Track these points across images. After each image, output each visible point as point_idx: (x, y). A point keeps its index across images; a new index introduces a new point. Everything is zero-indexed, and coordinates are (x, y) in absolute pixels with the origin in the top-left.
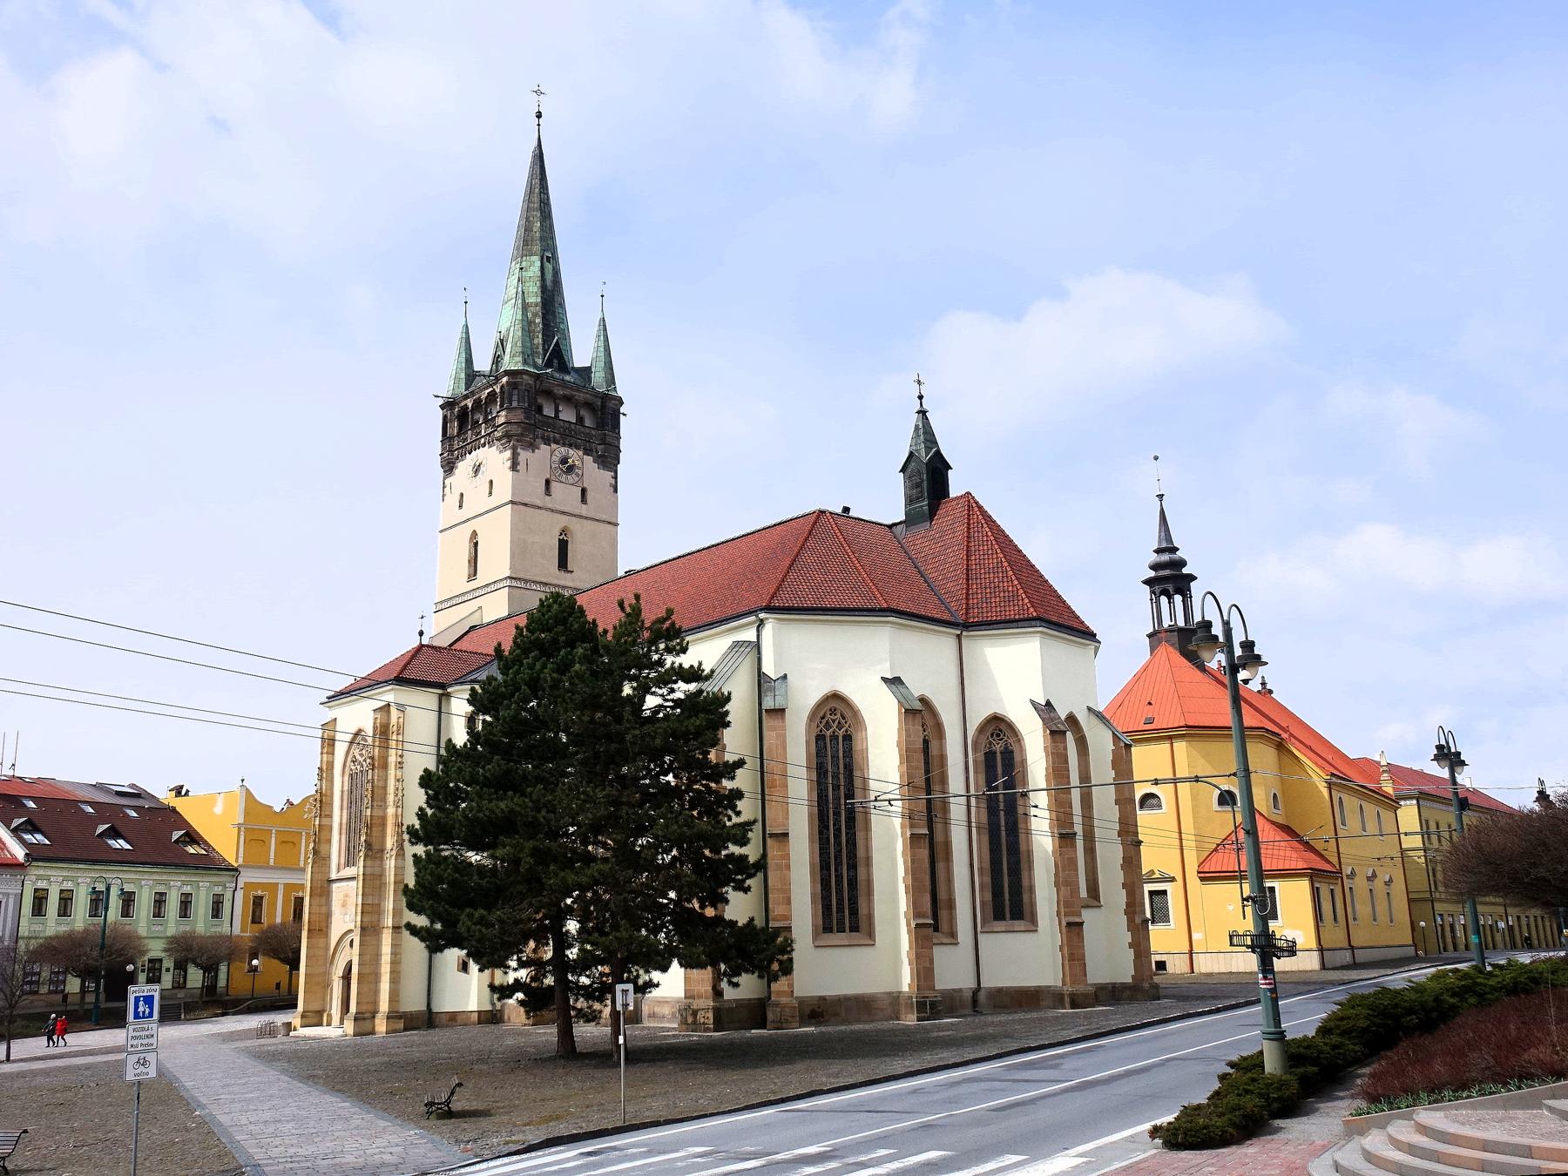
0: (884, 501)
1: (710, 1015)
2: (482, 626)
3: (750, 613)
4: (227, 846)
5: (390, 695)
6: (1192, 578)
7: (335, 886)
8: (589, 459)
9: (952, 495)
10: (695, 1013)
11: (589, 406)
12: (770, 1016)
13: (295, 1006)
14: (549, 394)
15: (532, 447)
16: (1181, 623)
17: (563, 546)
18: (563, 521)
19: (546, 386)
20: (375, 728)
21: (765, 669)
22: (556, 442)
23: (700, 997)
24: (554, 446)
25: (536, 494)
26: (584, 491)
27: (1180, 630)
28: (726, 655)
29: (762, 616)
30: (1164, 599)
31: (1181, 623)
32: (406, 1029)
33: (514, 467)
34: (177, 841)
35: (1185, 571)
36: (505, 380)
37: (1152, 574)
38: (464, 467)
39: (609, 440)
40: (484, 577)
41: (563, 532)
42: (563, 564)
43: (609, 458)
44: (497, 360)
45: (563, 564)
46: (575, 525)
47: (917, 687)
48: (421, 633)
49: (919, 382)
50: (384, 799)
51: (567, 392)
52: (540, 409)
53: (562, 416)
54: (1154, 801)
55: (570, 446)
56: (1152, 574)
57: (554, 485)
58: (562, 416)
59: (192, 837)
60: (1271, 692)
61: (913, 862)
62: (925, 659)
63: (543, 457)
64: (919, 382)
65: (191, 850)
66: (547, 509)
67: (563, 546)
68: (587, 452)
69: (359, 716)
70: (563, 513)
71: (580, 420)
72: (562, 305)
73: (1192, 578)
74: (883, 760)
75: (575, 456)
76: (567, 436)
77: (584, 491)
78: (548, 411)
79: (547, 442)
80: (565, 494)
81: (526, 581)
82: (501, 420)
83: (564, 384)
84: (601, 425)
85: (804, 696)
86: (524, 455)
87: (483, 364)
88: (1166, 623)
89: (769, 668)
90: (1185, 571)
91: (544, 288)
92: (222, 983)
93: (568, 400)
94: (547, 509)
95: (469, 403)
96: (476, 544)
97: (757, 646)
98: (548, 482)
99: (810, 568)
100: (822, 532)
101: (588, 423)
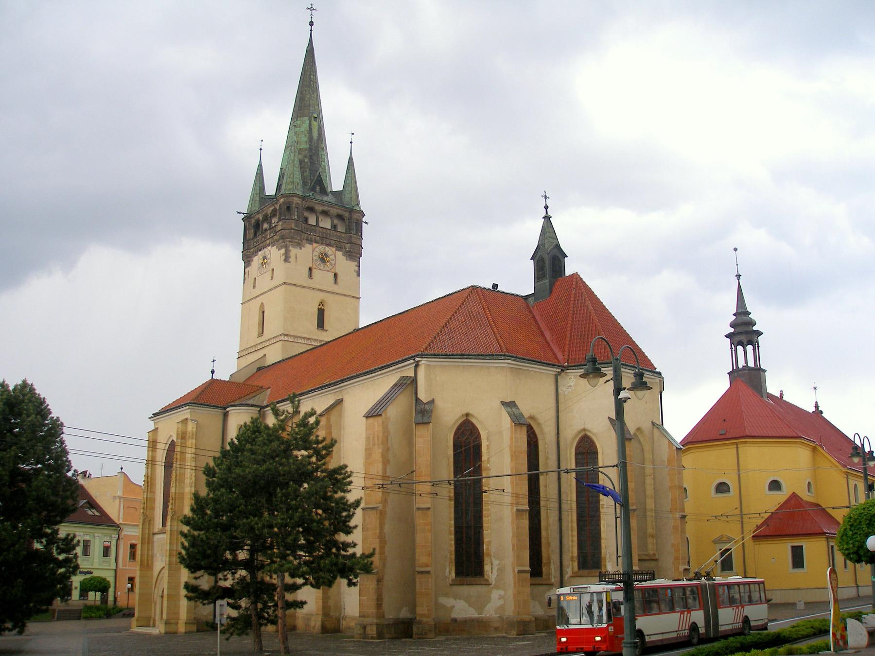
0: (520, 281)
1: (374, 628)
2: (265, 367)
3: (410, 359)
4: (113, 510)
5: (185, 413)
6: (759, 333)
7: (156, 537)
8: (339, 254)
9: (567, 274)
10: (365, 628)
11: (340, 217)
12: (415, 629)
13: (133, 615)
14: (311, 209)
15: (300, 245)
16: (751, 364)
17: (321, 313)
18: (322, 296)
19: (310, 204)
20: (178, 435)
21: (419, 396)
22: (316, 242)
23: (368, 616)
24: (315, 245)
25: (301, 277)
26: (335, 275)
27: (751, 369)
28: (392, 388)
29: (417, 359)
30: (740, 348)
31: (751, 364)
32: (198, 631)
33: (287, 259)
34: (82, 507)
35: (755, 328)
36: (282, 200)
37: (732, 330)
38: (257, 260)
39: (354, 240)
40: (269, 332)
41: (322, 303)
42: (321, 324)
43: (354, 253)
44: (279, 187)
45: (321, 324)
46: (330, 299)
47: (526, 409)
48: (213, 372)
49: (546, 197)
50: (183, 482)
51: (325, 208)
52: (306, 219)
53: (321, 224)
54: (725, 488)
55: (328, 245)
56: (732, 330)
57: (314, 271)
58: (321, 224)
59: (92, 504)
60: (821, 412)
61: (518, 528)
62: (534, 390)
63: (306, 254)
64: (546, 197)
65: (90, 513)
66: (310, 288)
67: (321, 313)
68: (339, 248)
69: (169, 429)
70: (321, 290)
71: (334, 227)
72: (324, 149)
73: (759, 333)
74: (501, 458)
75: (330, 250)
76: (324, 238)
77: (335, 275)
78: (312, 221)
79: (310, 241)
80: (322, 278)
81: (295, 337)
82: (279, 228)
83: (322, 203)
84: (349, 230)
85: (449, 415)
86: (294, 251)
87: (270, 189)
88: (741, 364)
89: (423, 396)
90: (755, 328)
91: (311, 139)
92: (111, 598)
93: (325, 213)
94: (310, 288)
95: (260, 217)
96: (263, 312)
97: (414, 381)
98: (310, 269)
99: (469, 324)
100: (481, 301)
101: (340, 229)
